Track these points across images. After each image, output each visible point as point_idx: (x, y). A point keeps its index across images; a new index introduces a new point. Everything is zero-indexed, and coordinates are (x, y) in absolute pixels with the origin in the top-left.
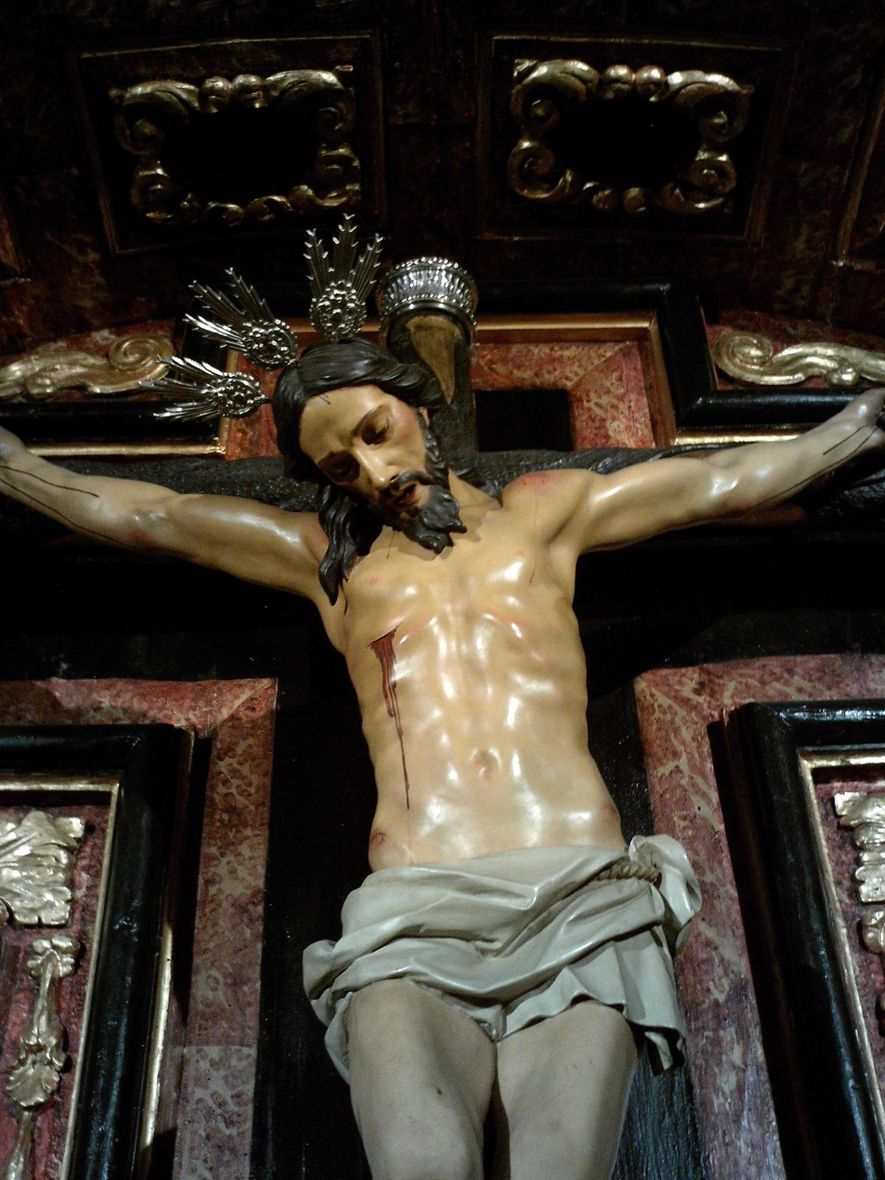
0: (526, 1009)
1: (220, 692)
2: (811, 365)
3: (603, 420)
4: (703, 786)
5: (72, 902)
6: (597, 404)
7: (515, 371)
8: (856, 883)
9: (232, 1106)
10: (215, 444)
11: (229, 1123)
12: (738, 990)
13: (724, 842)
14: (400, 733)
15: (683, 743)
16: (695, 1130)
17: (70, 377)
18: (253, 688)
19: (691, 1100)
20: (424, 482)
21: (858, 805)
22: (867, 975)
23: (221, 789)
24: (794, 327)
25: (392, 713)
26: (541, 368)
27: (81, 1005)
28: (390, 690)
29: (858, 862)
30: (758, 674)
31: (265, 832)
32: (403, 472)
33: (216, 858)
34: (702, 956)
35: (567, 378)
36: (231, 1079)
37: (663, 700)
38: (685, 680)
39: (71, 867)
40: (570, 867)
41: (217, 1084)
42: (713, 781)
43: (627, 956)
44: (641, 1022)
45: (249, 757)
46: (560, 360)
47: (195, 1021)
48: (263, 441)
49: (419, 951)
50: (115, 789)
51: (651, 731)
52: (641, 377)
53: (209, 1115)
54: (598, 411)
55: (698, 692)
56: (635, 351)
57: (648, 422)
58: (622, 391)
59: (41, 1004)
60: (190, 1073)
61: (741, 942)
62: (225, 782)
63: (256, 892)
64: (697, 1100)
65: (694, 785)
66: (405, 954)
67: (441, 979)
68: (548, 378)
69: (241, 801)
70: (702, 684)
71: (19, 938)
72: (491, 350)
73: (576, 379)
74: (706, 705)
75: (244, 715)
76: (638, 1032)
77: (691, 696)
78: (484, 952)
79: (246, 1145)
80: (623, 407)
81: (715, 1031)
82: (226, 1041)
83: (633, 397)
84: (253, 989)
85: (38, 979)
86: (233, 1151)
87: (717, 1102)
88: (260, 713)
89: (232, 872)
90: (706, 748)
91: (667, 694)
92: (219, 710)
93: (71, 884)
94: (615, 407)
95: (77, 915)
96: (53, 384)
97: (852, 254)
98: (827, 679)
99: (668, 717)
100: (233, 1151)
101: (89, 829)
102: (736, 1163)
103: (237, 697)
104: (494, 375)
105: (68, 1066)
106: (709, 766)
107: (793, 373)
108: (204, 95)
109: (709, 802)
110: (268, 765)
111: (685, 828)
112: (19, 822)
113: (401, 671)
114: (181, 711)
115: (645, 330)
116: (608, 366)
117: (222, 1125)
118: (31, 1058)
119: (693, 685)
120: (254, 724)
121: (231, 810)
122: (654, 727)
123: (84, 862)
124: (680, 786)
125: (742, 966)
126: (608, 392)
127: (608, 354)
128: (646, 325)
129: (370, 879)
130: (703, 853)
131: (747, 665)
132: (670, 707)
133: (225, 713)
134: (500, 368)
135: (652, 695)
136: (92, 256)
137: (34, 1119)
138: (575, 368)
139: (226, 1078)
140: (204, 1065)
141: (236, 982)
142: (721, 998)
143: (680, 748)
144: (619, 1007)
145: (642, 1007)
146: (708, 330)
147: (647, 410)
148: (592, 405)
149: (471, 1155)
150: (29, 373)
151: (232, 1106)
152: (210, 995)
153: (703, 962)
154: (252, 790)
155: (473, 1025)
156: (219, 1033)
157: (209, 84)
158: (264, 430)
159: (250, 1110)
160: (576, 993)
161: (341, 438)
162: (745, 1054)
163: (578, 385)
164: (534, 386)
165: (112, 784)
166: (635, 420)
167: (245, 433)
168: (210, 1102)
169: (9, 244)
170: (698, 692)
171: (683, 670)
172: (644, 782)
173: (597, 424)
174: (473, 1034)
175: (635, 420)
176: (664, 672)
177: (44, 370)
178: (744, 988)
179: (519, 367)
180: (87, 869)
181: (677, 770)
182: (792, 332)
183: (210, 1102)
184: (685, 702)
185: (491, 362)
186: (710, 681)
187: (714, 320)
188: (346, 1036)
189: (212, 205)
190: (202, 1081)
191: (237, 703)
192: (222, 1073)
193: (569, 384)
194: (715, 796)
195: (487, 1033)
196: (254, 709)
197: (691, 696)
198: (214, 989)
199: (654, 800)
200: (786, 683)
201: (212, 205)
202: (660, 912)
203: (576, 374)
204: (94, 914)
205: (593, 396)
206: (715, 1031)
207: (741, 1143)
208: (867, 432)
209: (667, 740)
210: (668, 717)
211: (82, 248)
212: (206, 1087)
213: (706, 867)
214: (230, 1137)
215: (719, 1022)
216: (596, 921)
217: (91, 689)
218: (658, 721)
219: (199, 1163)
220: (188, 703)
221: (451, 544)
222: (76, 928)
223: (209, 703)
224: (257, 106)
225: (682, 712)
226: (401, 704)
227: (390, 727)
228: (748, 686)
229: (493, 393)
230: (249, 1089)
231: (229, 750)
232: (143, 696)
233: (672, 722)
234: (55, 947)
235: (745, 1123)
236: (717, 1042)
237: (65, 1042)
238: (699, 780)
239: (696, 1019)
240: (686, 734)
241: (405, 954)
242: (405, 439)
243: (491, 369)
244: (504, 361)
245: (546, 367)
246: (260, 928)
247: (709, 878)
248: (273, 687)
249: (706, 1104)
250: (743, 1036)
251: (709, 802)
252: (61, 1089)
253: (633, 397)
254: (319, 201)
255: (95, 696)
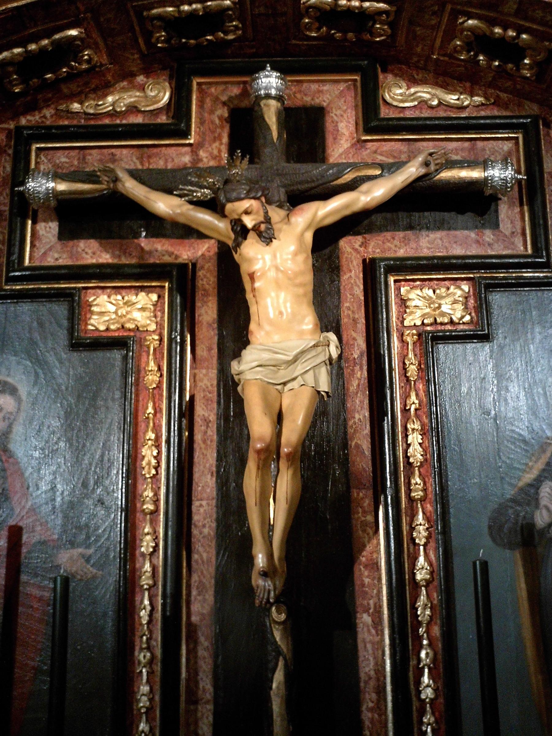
0: (289, 386)
1: (198, 244)
2: (420, 97)
3: (337, 122)
4: (358, 282)
5: (157, 323)
6: (336, 115)
7: (304, 98)
8: (404, 319)
9: (210, 388)
10: (190, 139)
11: (210, 393)
12: (361, 355)
13: (363, 303)
14: (257, 303)
15: (354, 267)
16: (344, 397)
17: (131, 102)
18: (209, 243)
19: (344, 388)
20: (262, 222)
21: (408, 292)
22: (403, 350)
23: (201, 282)
24: (418, 75)
25: (254, 296)
26: (314, 96)
27: (163, 357)
28: (253, 290)
29: (405, 312)
30: (382, 239)
31: (216, 298)
32: (258, 221)
33: (200, 307)
34: (352, 343)
35: (324, 101)
36: (210, 379)
37: (349, 250)
38: (357, 241)
39: (155, 310)
40: (303, 346)
41: (205, 381)
42: (362, 281)
43: (317, 371)
44: (319, 390)
45: (209, 270)
46: (322, 92)
47: (198, 362)
48: (207, 133)
49: (262, 371)
50: (167, 285)
51: (344, 262)
52: (353, 101)
53: (204, 390)
54: (335, 118)
55: (360, 246)
56: (352, 87)
57: (354, 124)
58: (345, 108)
59: (151, 357)
60: (197, 377)
61: (364, 338)
62: (202, 280)
63: (214, 320)
64: (346, 388)
65: (355, 282)
66: (257, 373)
67: (266, 380)
68: (317, 101)
69: (207, 287)
70: (362, 243)
71: (140, 335)
72: (295, 86)
73: (328, 101)
74: (363, 252)
75: (207, 254)
76: (319, 392)
77: (359, 248)
78: (279, 369)
79: (215, 399)
80: (345, 116)
81: (353, 367)
82: (207, 368)
83: (349, 111)
84: (215, 351)
85: (149, 347)
86: (212, 401)
87: (351, 389)
88: (212, 253)
89: (206, 312)
90: (361, 268)
91: (349, 247)
92: (198, 251)
93: (155, 316)
94: (342, 116)
95: (158, 326)
96: (125, 105)
97: (438, 54)
98: (406, 241)
99: (350, 256)
100: (212, 401)
101: (159, 297)
102: (355, 407)
103: (203, 246)
104: (296, 99)
105: (161, 376)
106: (361, 275)
107: (412, 101)
108: (179, 12)
109: (360, 289)
110: (215, 274)
111: (351, 298)
112: (137, 295)
113: (257, 285)
114: (185, 251)
115: (356, 79)
116: (341, 94)
117: (208, 393)
118: (150, 373)
119: (359, 243)
120: (210, 258)
121: (205, 290)
122: (345, 260)
123: (158, 308)
124: (351, 282)
125: (364, 346)
126: (340, 108)
127: (341, 89)
128: (356, 78)
129: (249, 347)
130: (355, 307)
131: (379, 236)
132: (351, 252)
133: (200, 253)
134: (298, 96)
135: (345, 247)
136: (136, 56)
137: (153, 391)
138: (328, 96)
139: (208, 380)
140: (201, 375)
141: (210, 349)
142: (356, 356)
143: (352, 268)
144: (313, 387)
145: (319, 385)
146: (381, 77)
147: (354, 118)
148: (333, 115)
149: (272, 435)
150: (114, 100)
151: (210, 388)
152: (202, 353)
153: (352, 345)
154: (211, 283)
155: (275, 390)
156: (205, 365)
157: (182, 8)
158: (207, 127)
159: (216, 389)
160: (302, 384)
161: (238, 215)
162: (361, 374)
163: (328, 105)
164: (311, 105)
165: (165, 283)
166: (349, 123)
167: (200, 129)
168: (204, 387)
169: (105, 57)
170: (360, 246)
171: (357, 237)
172: (339, 281)
173: (334, 125)
174: (275, 393)
175: (349, 123)
176: (350, 237)
177: (119, 99)
178: (363, 353)
179: (306, 95)
180: (160, 311)
181: (351, 277)
182: (416, 77)
183: (204, 387)
184: (356, 250)
185: (295, 93)
186: (366, 242)
187: (384, 71)
188: (243, 389)
189: (184, 40)
190: (201, 380)
191: (204, 249)
192: (207, 378)
193: (325, 104)
194: (362, 287)
195: (280, 392)
196: (209, 252)
197: (359, 248)
198: (203, 351)
199: (342, 288)
200: (392, 243)
201: (184, 40)
202: (327, 357)
203: (328, 99)
204: (164, 327)
205: (334, 110)
206: (353, 367)
207: (357, 401)
208: (420, 169)
209: (348, 265)
210: (350, 256)
211: (133, 54)
212: (202, 382)
213: (356, 312)
214: (211, 397)
215: (355, 364)
216: (309, 362)
217: (154, 242)
218: (346, 258)
219: (202, 404)
220: (187, 248)
221: (272, 241)
222: (158, 331)
223: (194, 249)
224: (201, 14)
225: (354, 254)
226: (257, 294)
227: (253, 300)
228: (378, 244)
229: (295, 108)
230: (215, 383)
231: (202, 268)
232: (172, 245)
233: (351, 258)
234: (153, 339)
235: (359, 395)
236: (353, 371)
237: (160, 369)
238: (357, 281)
239: (348, 363)
240: (355, 263)
241: (257, 373)
242: (257, 213)
243: (295, 96)
244: (300, 91)
245: (317, 95)
246: (216, 332)
247: (356, 316)
248: (215, 243)
249: (348, 389)
250: (361, 369)
251: (360, 289)
252: (160, 384)
253: (349, 111)
254: (226, 37)
255: (155, 245)
